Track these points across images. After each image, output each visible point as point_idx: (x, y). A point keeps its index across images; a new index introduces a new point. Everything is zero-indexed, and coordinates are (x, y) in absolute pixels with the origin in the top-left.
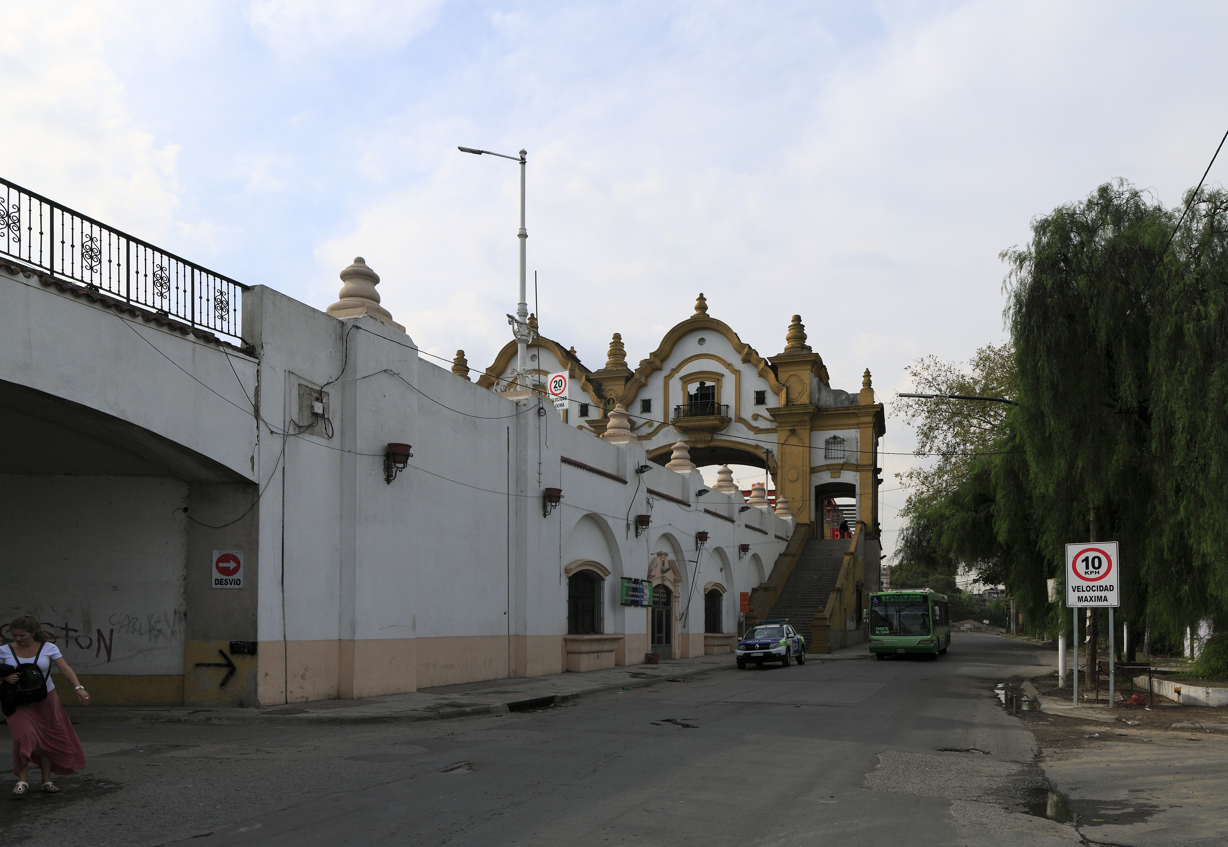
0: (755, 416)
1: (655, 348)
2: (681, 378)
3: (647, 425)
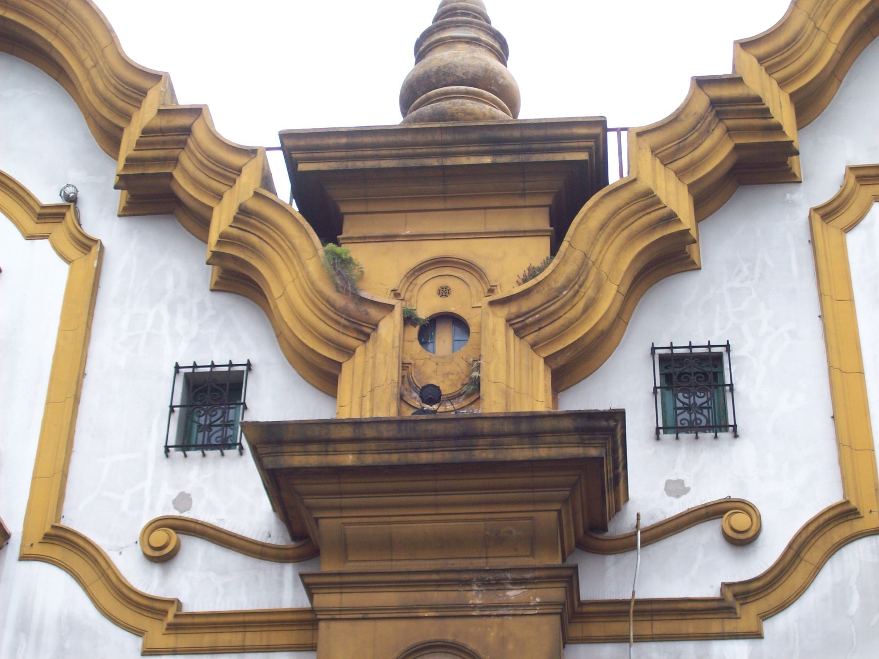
0: (159, 537)
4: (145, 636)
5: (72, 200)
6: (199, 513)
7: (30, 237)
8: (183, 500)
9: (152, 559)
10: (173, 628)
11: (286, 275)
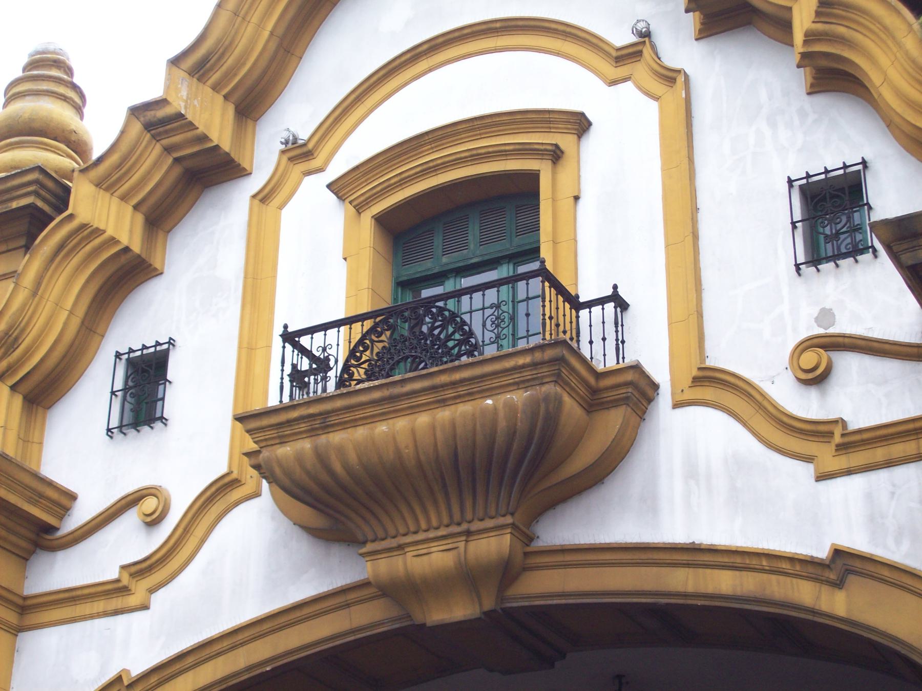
0: (809, 359)
2: (337, 187)
4: (815, 462)
5: (646, 35)
6: (844, 326)
7: (613, 83)
8: (826, 316)
9: (807, 383)
10: (843, 448)
11: (884, 60)
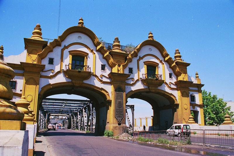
0: (101, 76)
1: (61, 35)
3: (131, 79)
